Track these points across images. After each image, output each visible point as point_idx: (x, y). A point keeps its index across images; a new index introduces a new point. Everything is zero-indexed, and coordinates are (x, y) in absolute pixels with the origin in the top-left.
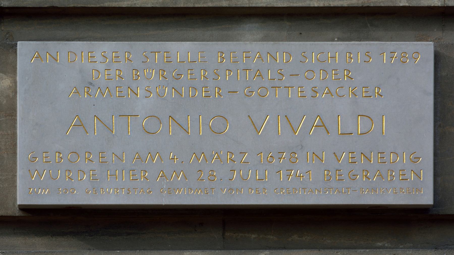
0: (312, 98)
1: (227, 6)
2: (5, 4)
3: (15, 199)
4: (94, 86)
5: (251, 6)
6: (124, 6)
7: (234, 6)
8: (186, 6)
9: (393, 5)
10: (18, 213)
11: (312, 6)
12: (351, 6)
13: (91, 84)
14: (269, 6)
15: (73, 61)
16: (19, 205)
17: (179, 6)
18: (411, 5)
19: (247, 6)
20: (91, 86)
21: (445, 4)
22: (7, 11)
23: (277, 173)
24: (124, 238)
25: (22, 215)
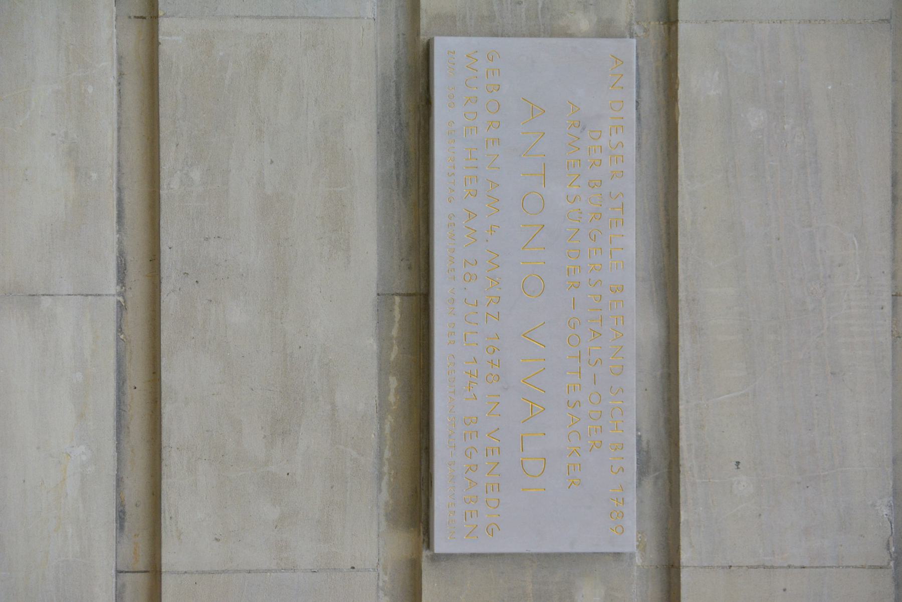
0: (567, 401)
1: (680, 298)
2: (681, 4)
3: (442, 34)
4: (581, 132)
5: (680, 327)
6: (679, 171)
7: (680, 306)
8: (680, 247)
9: (681, 502)
10: (423, 38)
11: (680, 403)
12: (680, 450)
13: (584, 129)
14: (680, 348)
15: (600, 397)
16: (433, 38)
17: (679, 239)
18: (681, 525)
19: (680, 323)
20: (580, 128)
21: (684, 566)
22: (673, 28)
23: (476, 301)
24: (393, 170)
25: (422, 37)
